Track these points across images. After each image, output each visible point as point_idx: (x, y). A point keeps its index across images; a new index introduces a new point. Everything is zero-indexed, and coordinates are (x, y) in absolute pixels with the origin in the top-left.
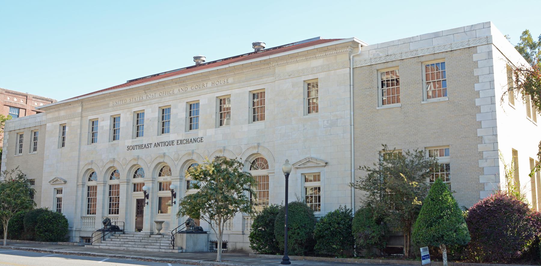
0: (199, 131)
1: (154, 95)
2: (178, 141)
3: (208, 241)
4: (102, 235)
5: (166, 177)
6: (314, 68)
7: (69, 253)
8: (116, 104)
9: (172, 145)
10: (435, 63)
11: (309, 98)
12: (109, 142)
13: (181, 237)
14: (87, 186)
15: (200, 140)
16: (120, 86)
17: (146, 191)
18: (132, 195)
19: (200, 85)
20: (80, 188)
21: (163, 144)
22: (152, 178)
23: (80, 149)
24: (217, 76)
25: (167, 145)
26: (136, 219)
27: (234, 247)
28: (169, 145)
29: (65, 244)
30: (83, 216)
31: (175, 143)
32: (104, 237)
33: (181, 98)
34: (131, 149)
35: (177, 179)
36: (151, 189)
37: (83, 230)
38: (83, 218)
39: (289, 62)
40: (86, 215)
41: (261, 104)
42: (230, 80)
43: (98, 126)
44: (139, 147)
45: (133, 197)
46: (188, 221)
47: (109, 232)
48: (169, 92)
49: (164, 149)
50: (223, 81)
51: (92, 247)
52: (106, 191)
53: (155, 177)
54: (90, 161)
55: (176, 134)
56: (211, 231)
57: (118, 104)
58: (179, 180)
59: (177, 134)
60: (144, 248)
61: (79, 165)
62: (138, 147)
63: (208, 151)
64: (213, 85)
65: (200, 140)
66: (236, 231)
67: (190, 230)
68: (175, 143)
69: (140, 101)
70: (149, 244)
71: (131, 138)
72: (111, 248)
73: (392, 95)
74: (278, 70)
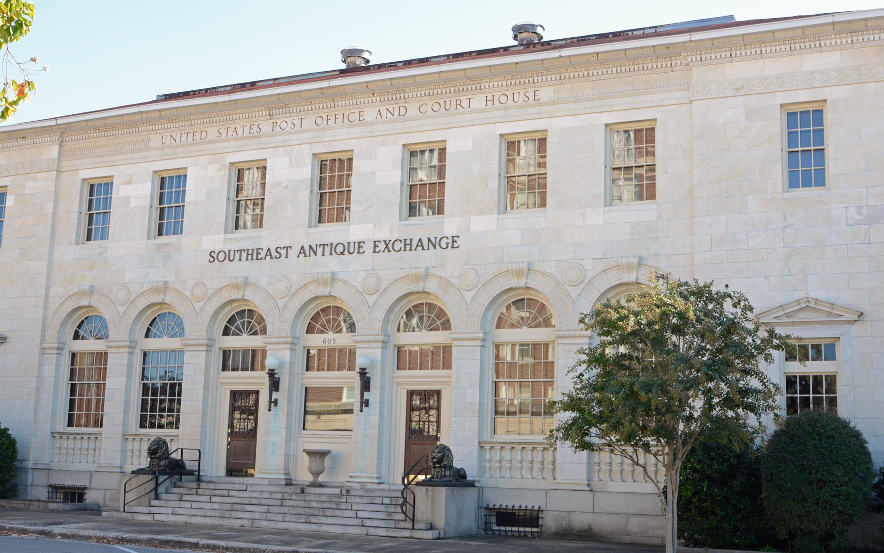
0: (446, 220)
1: (297, 122)
2: (377, 243)
3: (479, 507)
4: (152, 485)
5: (330, 335)
6: (813, 73)
7: (116, 538)
8: (172, 141)
9: (359, 253)
11: (90, 212)
12: (148, 238)
13: (428, 496)
14: (493, 343)
15: (448, 244)
17: (273, 370)
18: (218, 378)
19: (164, 137)
20: (51, 358)
21: (327, 249)
22: (208, 339)
23: (51, 254)
24: (103, 133)
25: (342, 253)
26: (229, 444)
27: (564, 523)
28: (346, 252)
29: (15, 505)
30: (57, 431)
31: (368, 248)
32: (156, 489)
34: (221, 258)
35: (374, 341)
36: (287, 366)
37: (59, 468)
38: (58, 436)
39: (241, 118)
40: (136, 431)
41: (340, 185)
42: (545, 94)
43: (114, 195)
44: (248, 254)
45: (222, 384)
46: (155, 445)
47: (167, 477)
48: (346, 117)
49: (331, 263)
50: (522, 95)
51: (129, 518)
52: (134, 367)
53: (136, 338)
54: (88, 287)
55: (373, 224)
56: (482, 479)
57: (178, 140)
58: (380, 344)
59: (375, 225)
60: (306, 523)
61: (47, 296)
62: (244, 255)
63: (477, 272)
64: (490, 103)
65: (448, 244)
66: (567, 482)
67: (445, 476)
68: (368, 248)
69: (251, 136)
70: (315, 513)
71: (223, 232)
72: (195, 520)
74: (698, 73)
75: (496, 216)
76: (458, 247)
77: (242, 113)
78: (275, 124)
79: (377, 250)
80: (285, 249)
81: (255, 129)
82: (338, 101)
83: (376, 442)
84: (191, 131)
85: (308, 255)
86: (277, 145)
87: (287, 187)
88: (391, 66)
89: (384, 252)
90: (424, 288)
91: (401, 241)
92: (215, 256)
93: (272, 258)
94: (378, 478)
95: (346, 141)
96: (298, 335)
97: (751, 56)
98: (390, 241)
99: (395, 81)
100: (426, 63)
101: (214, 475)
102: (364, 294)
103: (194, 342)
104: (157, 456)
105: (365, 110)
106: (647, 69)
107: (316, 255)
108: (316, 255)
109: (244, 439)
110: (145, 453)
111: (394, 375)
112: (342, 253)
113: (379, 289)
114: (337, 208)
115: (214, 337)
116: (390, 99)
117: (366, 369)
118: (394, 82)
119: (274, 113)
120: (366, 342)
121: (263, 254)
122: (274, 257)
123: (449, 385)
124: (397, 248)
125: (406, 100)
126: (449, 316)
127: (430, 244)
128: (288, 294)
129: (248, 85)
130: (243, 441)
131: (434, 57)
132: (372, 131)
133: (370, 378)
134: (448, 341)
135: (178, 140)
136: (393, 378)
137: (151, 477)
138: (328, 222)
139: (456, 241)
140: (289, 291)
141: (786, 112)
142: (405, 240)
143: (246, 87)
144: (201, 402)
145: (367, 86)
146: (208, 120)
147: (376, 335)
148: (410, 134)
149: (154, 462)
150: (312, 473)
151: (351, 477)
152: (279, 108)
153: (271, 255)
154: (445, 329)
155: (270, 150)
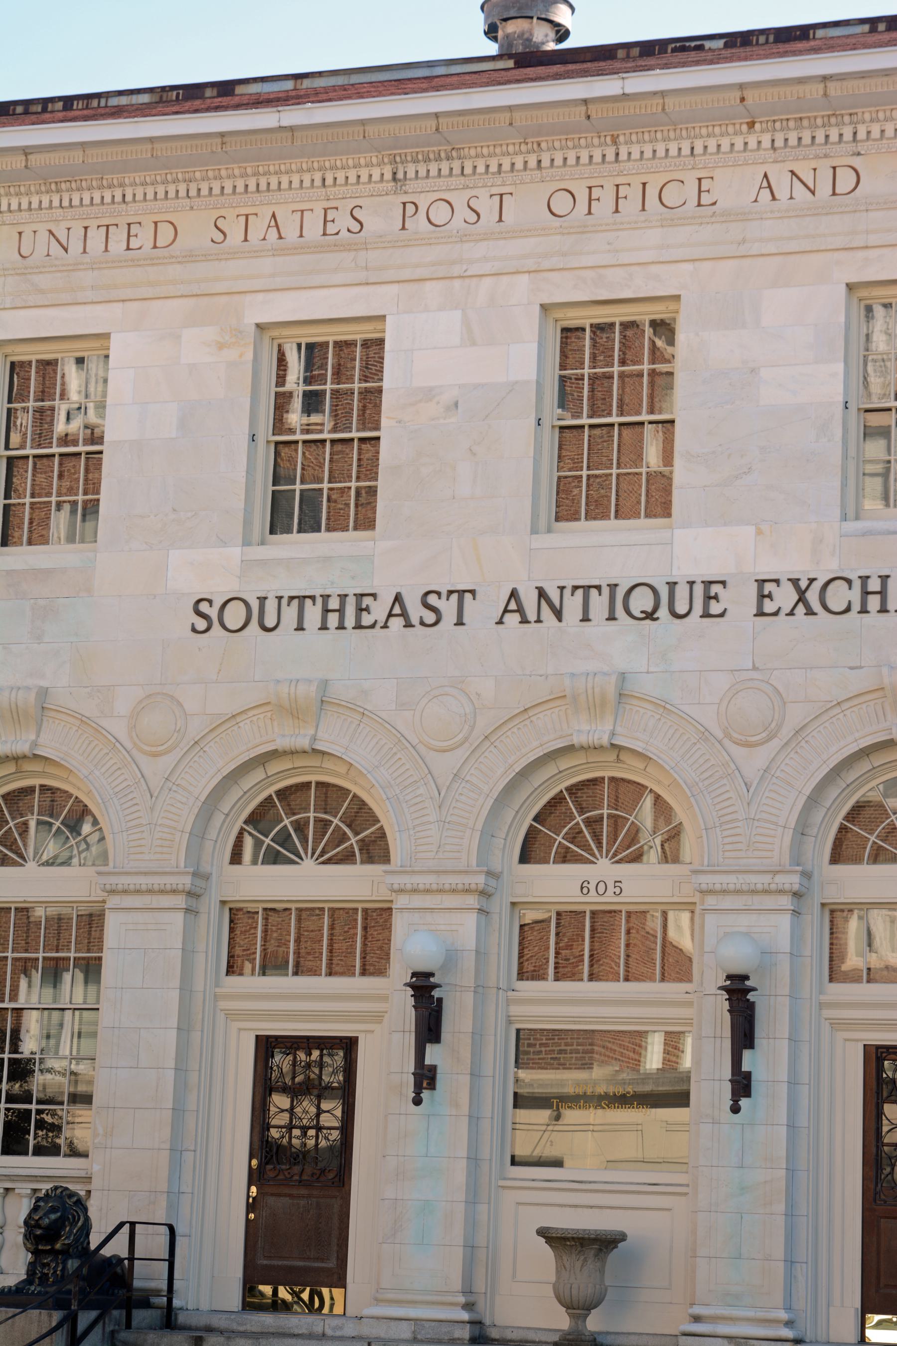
1: (487, 206)
8: (56, 249)
9: (706, 615)
10: (617, 320)
16: (797, 53)
21: (599, 604)
25: (650, 616)
33: (793, 246)
35: (766, 892)
36: (469, 962)
44: (326, 611)
48: (652, 193)
55: (751, 530)
57: (75, 246)
59: (759, 532)
62: (313, 613)
73: (330, 482)
75: (238, 550)
76: (722, 615)
77: (300, 171)
78: (410, 209)
79: (769, 606)
80: (455, 597)
81: (343, 221)
82: (629, 142)
83: (781, 1207)
84: (123, 221)
85: (532, 616)
86: (419, 273)
87: (456, 405)
88: (683, 49)
89: (791, 613)
90: (314, 739)
91: (849, 582)
92: (213, 613)
93: (408, 625)
94: (789, 1324)
95: (654, 269)
96: (497, 867)
97: (666, 161)
98: (812, 581)
99: (838, 84)
100: (800, 45)
101: (205, 1306)
102: (726, 742)
103: (143, 882)
104: (58, 1246)
105: (717, 174)
106: (428, 177)
107: (560, 620)
108: (560, 620)
109: (304, 1191)
110: (15, 1235)
111: (824, 998)
112: (650, 616)
113: (779, 727)
114: (32, 504)
115: (205, 868)
116: (807, 140)
117: (746, 978)
118: (834, 88)
119: (411, 174)
120: (738, 892)
121: (379, 611)
122: (415, 620)
123: (380, 1022)
124: (836, 604)
125: (861, 148)
126: (384, 822)
127: (557, 603)
128: (466, 739)
129: (209, 93)
130: (300, 1197)
131: (825, 25)
132: (744, 241)
133: (440, 1000)
134: (382, 894)
135: (75, 246)
136: (216, 998)
137: (57, 1316)
138: (30, 543)
139: (716, 597)
140: (473, 728)
141: (863, 303)
142: (865, 579)
143: (202, 97)
144: (171, 1073)
145: (743, 99)
146: (182, 188)
147: (776, 873)
148: (872, 254)
149: (44, 1265)
150: (569, 1306)
151: (697, 1319)
152: (427, 160)
153: (404, 614)
154: (369, 859)
155: (395, 288)
